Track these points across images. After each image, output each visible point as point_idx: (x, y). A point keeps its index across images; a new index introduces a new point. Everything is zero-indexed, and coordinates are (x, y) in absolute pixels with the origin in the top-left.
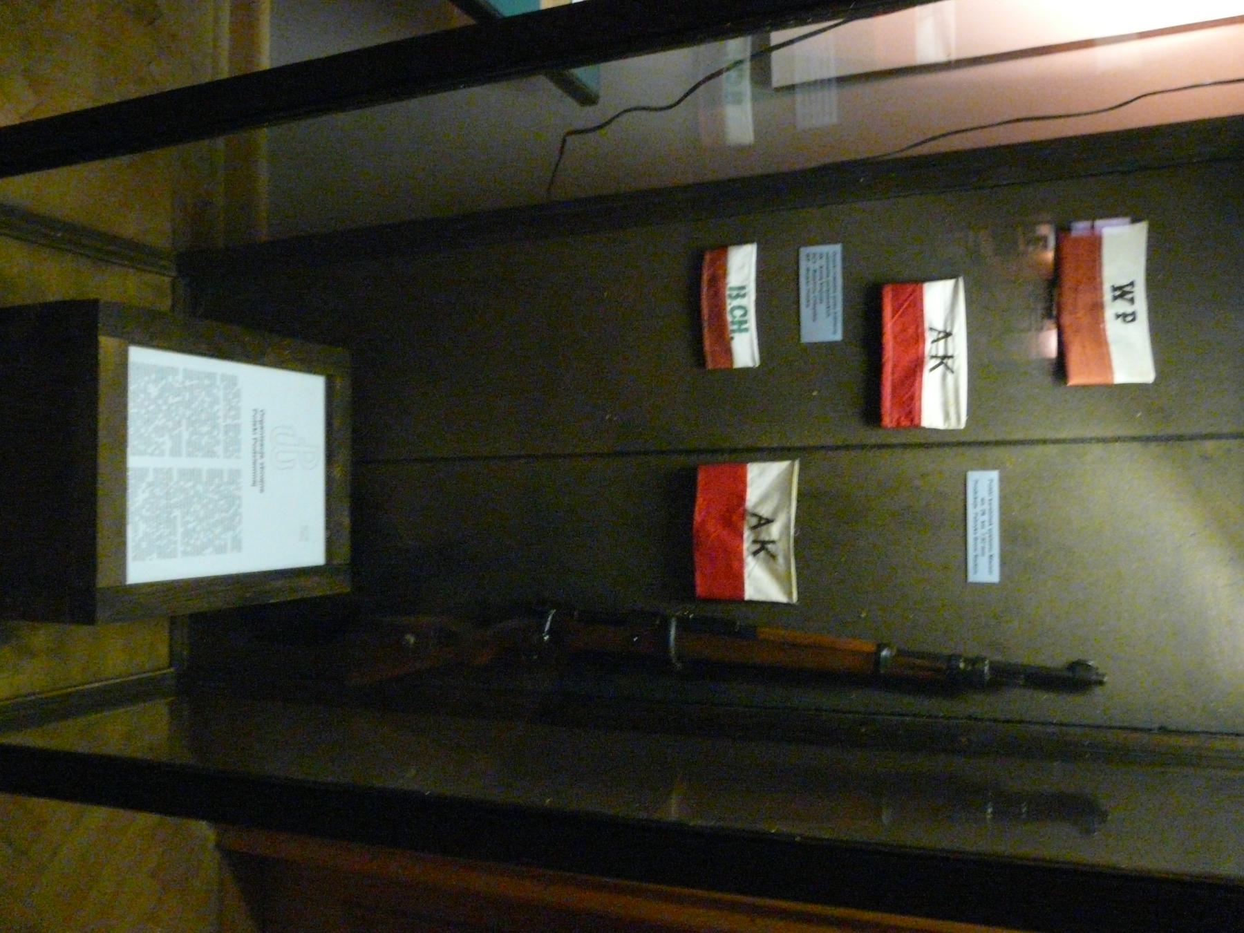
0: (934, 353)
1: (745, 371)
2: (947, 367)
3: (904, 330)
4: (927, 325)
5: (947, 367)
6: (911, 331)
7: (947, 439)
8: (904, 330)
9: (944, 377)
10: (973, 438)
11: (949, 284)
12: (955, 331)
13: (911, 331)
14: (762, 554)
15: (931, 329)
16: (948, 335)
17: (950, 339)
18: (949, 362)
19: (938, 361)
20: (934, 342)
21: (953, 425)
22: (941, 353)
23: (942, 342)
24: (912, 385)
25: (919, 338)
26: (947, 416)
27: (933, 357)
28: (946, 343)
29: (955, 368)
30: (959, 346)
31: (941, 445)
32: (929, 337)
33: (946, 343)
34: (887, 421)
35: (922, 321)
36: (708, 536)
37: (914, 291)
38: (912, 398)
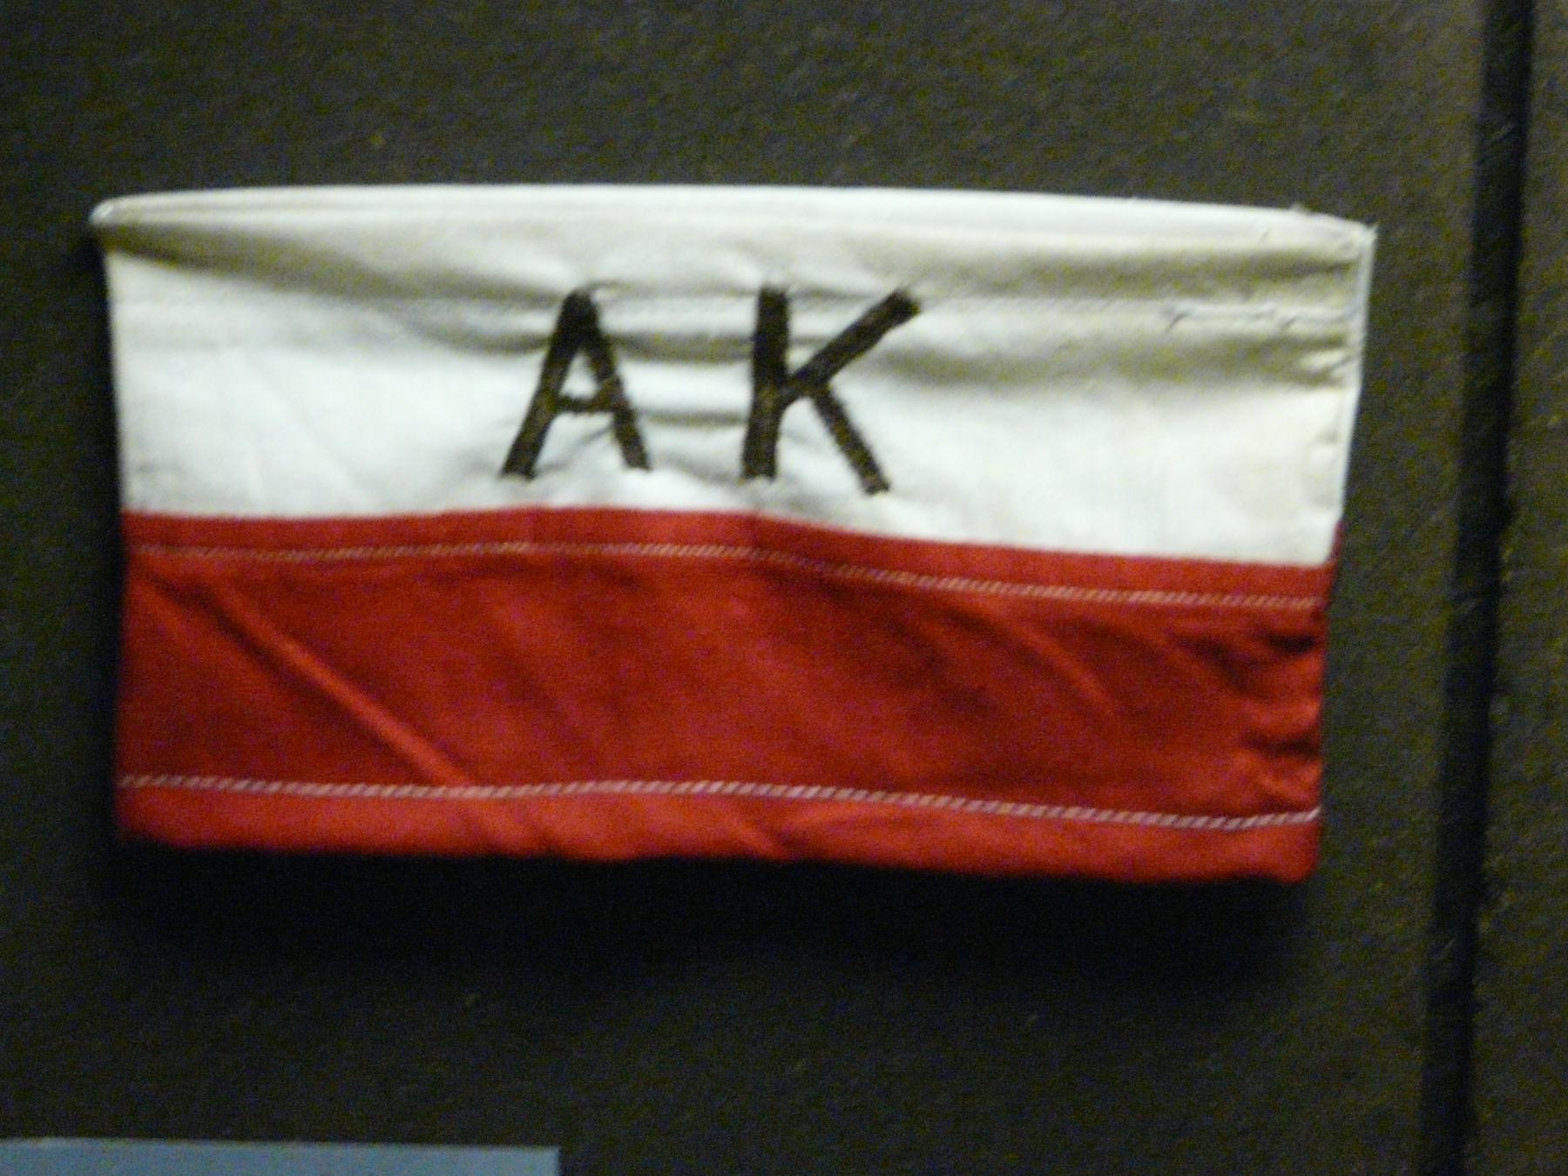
0: (729, 444)
1: (1446, 434)
2: (856, 342)
3: (518, 683)
4: (491, 495)
5: (856, 342)
6: (523, 621)
7: (1449, 378)
8: (518, 683)
9: (937, 372)
10: (1453, 171)
11: (139, 297)
12: (559, 274)
13: (523, 621)
14: (741, 318)
15: (523, 457)
16: (579, 331)
17: (616, 320)
18: (813, 326)
19: (801, 415)
20: (635, 454)
21: (1342, 311)
22: (730, 388)
23: (644, 383)
24: (965, 620)
25: (588, 561)
26: (1269, 361)
27: (760, 456)
28: (650, 348)
29: (879, 287)
30: (679, 244)
31: (1489, 516)
32: (585, 473)
33: (650, 348)
34: (1263, 837)
35: (459, 526)
36: (1489, 1091)
37: (192, 595)
38: (1096, 636)
